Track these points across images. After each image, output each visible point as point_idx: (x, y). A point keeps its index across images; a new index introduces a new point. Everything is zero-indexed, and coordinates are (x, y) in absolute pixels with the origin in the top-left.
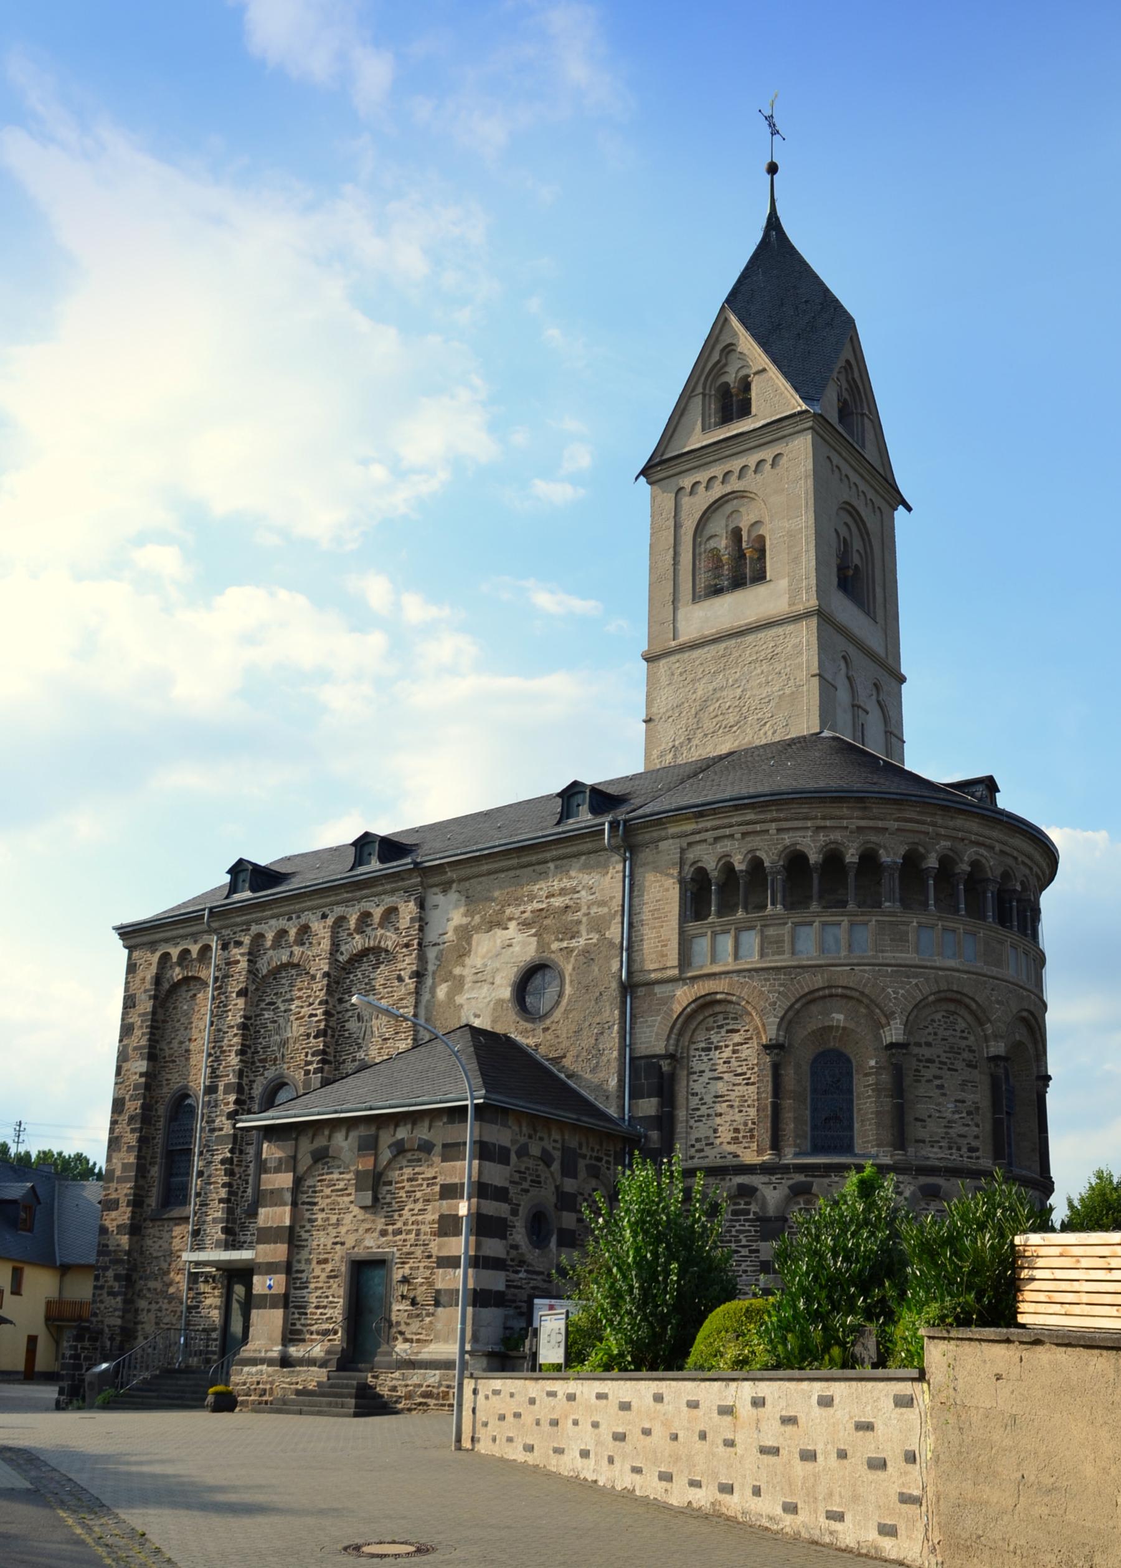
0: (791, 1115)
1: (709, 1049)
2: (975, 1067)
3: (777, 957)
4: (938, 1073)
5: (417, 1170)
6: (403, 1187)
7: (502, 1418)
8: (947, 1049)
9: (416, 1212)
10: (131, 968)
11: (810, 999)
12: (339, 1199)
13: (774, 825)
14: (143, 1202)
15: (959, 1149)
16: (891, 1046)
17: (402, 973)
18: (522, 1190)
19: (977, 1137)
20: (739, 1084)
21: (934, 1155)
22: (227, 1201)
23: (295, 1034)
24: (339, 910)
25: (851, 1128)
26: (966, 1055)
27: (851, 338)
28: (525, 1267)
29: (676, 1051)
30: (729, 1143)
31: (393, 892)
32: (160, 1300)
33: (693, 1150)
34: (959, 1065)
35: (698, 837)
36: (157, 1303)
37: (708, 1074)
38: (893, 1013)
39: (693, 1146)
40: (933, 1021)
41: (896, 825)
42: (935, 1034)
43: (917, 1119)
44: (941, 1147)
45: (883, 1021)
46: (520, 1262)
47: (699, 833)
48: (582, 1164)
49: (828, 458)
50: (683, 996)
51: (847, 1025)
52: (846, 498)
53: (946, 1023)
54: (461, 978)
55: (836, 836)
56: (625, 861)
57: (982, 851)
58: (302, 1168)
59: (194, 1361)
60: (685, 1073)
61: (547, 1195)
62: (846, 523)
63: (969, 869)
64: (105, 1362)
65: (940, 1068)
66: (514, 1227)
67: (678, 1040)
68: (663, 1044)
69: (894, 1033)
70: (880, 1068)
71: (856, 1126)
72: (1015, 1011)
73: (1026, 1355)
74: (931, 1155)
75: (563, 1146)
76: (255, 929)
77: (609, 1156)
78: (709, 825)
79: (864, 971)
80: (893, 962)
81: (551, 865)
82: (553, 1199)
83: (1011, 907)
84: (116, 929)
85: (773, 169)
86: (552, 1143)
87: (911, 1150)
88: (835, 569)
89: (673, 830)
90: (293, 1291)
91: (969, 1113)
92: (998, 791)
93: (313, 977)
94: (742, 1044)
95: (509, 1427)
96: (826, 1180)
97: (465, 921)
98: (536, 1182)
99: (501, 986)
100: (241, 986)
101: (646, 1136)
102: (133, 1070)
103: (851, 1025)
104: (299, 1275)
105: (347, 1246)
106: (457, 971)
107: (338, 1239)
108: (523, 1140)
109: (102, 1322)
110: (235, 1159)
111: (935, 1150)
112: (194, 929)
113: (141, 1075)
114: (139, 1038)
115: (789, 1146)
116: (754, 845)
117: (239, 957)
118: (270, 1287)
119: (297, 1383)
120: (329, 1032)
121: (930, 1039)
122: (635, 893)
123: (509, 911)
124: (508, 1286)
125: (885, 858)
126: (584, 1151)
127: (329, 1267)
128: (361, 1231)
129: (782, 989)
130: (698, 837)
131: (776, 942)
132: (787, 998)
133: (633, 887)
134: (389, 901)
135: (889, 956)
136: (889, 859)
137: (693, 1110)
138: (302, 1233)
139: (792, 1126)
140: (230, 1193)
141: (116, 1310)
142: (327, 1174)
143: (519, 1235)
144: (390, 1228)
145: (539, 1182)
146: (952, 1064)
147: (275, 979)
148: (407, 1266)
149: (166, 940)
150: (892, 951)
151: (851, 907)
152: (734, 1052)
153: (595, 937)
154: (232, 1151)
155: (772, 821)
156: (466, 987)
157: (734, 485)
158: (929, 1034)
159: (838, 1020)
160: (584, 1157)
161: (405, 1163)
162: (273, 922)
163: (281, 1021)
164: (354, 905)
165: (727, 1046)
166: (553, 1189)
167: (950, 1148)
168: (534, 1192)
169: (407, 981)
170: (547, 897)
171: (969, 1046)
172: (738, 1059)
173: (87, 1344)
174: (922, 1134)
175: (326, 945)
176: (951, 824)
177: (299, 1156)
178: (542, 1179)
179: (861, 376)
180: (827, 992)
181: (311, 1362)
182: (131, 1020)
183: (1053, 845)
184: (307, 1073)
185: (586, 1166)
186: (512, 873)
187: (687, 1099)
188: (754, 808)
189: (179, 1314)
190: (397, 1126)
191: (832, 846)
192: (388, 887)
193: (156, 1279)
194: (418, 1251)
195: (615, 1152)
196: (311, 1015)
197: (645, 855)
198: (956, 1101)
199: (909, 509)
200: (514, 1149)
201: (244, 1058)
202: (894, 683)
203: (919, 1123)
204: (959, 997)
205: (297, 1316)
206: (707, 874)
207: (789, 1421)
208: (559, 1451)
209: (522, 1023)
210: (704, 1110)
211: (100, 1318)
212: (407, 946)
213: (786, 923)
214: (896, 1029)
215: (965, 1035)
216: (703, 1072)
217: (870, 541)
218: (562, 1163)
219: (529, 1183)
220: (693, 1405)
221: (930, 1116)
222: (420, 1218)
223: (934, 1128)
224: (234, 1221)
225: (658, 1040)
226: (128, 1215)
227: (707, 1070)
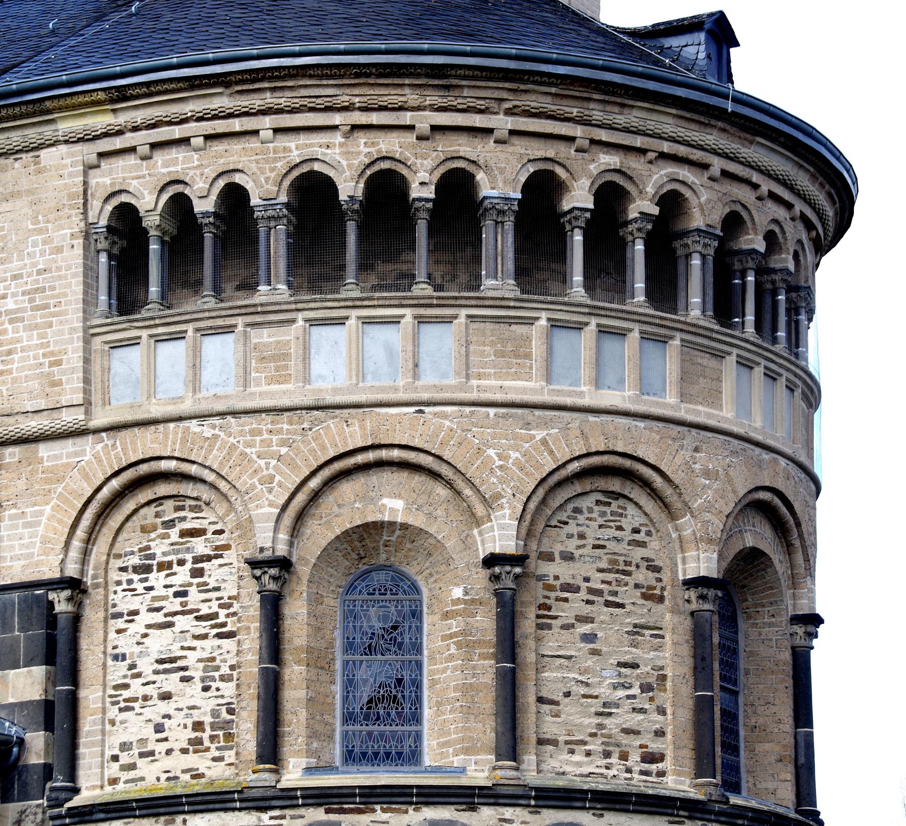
0: (301, 694)
1: (148, 569)
2: (661, 599)
3: (275, 387)
4: (587, 610)
8: (604, 565)
11: (345, 468)
13: (268, 122)
15: (624, 757)
20: (204, 637)
25: (416, 718)
26: (642, 576)
29: (82, 572)
30: (184, 751)
33: (116, 766)
34: (628, 595)
35: (118, 143)
37: (146, 618)
38: (498, 496)
39: (115, 758)
40: (577, 510)
42: (582, 536)
44: (588, 754)
45: (480, 510)
47: (120, 133)
50: (89, 464)
51: (410, 521)
55: (390, 144)
57: (685, 173)
60: (101, 615)
63: (655, 211)
65: (588, 602)
68: (55, 560)
69: (501, 535)
70: (473, 601)
71: (427, 713)
72: (741, 493)
74: (568, 769)
78: (139, 116)
79: (445, 416)
83: (744, 285)
87: (529, 759)
91: (646, 688)
92: (737, 44)
94: (209, 558)
101: (21, 742)
103: (417, 520)
111: (577, 758)
115: (297, 754)
116: (231, 161)
121: (571, 545)
125: (488, 188)
129: (283, 450)
130: (118, 143)
131: (274, 358)
135: (492, 386)
136: (494, 193)
137: (116, 687)
139: (303, 714)
146: (615, 594)
150: (498, 376)
151: (421, 289)
152: (197, 573)
159: (392, 510)
165: (181, 563)
167: (607, 755)
171: (647, 560)
172: (204, 588)
174: (551, 727)
176: (621, 119)
183: (839, 156)
187: (105, 665)
188: (227, 85)
198: (620, 664)
203: (546, 708)
204: (627, 463)
206: (140, 219)
210: (137, 688)
213: (293, 321)
214: (502, 527)
216: (135, 613)
221: (567, 694)
223: (576, 718)
227: (143, 609)
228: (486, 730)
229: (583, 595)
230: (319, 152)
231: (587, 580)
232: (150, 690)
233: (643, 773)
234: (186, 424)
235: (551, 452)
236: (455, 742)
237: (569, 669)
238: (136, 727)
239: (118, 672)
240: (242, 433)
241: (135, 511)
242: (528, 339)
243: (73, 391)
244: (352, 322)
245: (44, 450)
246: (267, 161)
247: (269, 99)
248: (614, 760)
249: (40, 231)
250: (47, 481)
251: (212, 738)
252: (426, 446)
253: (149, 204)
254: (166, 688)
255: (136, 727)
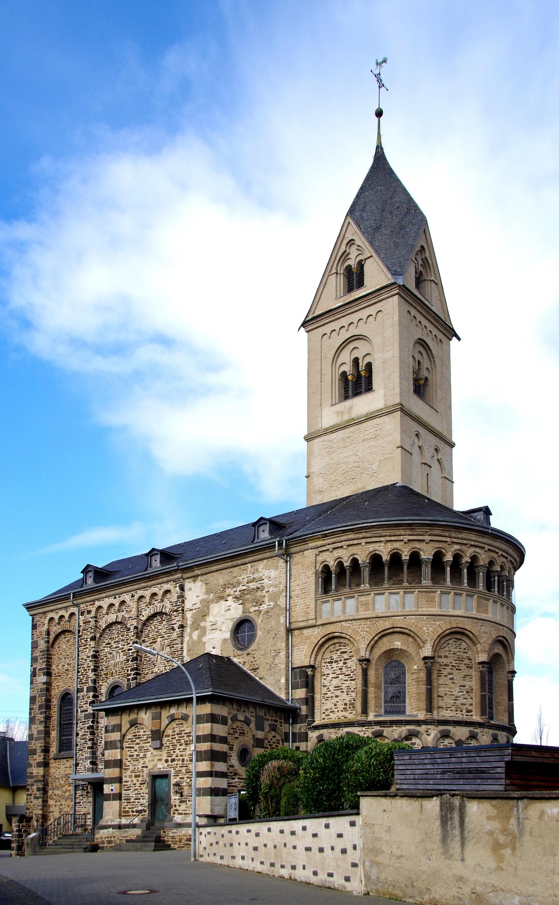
0: (373, 695)
1: (332, 662)
2: (472, 668)
5: (181, 729)
6: (175, 738)
7: (211, 844)
8: (456, 659)
9: (181, 750)
10: (34, 627)
11: (384, 634)
12: (144, 745)
13: (364, 540)
14: (49, 750)
15: (461, 711)
16: (425, 658)
17: (174, 626)
18: (235, 738)
19: (471, 705)
20: (347, 680)
21: (447, 714)
22: (92, 748)
23: (121, 660)
24: (140, 593)
25: (404, 702)
26: (467, 661)
27: (424, 231)
28: (238, 776)
29: (315, 664)
30: (342, 711)
31: (167, 582)
32: (61, 800)
33: (324, 715)
34: (463, 667)
35: (324, 548)
36: (60, 801)
37: (331, 676)
38: (427, 640)
39: (324, 713)
40: (448, 644)
41: (429, 538)
42: (450, 651)
43: (438, 696)
44: (451, 710)
45: (421, 644)
46: (235, 773)
47: (325, 546)
48: (267, 724)
49: (409, 312)
50: (317, 634)
51: (402, 648)
52: (420, 337)
53: (456, 645)
54: (205, 627)
55: (397, 545)
56: (287, 562)
57: (478, 550)
58: (124, 730)
59: (79, 830)
60: (320, 675)
61: (248, 740)
62: (420, 352)
63: (470, 560)
64: (34, 832)
66: (231, 756)
67: (316, 658)
68: (308, 660)
69: (427, 651)
70: (420, 670)
71: (407, 700)
72: (494, 637)
73: (393, 801)
74: (446, 715)
75: (256, 715)
76: (97, 604)
77: (281, 719)
78: (330, 541)
79: (412, 619)
80: (427, 613)
81: (249, 565)
82: (252, 742)
83: (494, 580)
84: (24, 605)
85: (379, 114)
86: (250, 714)
87: (435, 712)
88: (412, 381)
89: (311, 545)
90: (123, 792)
91: (467, 692)
93: (129, 629)
94: (348, 659)
95: (214, 849)
96: (391, 729)
97: (205, 597)
98: (242, 733)
99: (225, 631)
100: (92, 635)
101: (300, 709)
102: (39, 681)
103: (404, 648)
104: (126, 784)
105: (149, 768)
106: (202, 624)
107: (144, 765)
108: (234, 712)
109: (32, 812)
110: (95, 726)
111: (448, 712)
112: (65, 605)
113: (44, 683)
114: (41, 665)
117: (90, 619)
118: (112, 790)
119: (127, 837)
120: (139, 658)
121: (447, 654)
122: (292, 580)
123: (228, 591)
124: (228, 786)
125: (423, 556)
126: (268, 717)
127: (140, 779)
128: (155, 761)
129: (368, 629)
130: (324, 548)
131: (365, 604)
132: (370, 633)
133: (289, 575)
134: (166, 587)
135: (425, 610)
136: (425, 557)
137: (324, 694)
138: (127, 762)
139: (374, 701)
140: (93, 744)
141: (38, 806)
142: (138, 732)
143: (234, 760)
144: (170, 759)
145: (244, 734)
146: (459, 667)
147: (110, 630)
148: (178, 777)
149: (51, 611)
150: (426, 607)
151: (406, 584)
152: (345, 663)
153: (272, 604)
154: (93, 722)
155: (362, 538)
156: (207, 633)
157: (353, 331)
158: (446, 651)
160: (268, 720)
161: (175, 726)
162: (106, 600)
163: (114, 653)
164: (148, 590)
165: (341, 660)
166: (251, 737)
167: (457, 711)
168: (241, 738)
169: (177, 630)
170: (247, 583)
173: (24, 824)
174: (441, 704)
175: (134, 613)
177: (123, 724)
178: (245, 732)
179: (430, 255)
180: (391, 630)
181: (134, 826)
182: (36, 655)
184: (128, 680)
185: (269, 725)
186: (229, 570)
188: (353, 531)
189: (71, 806)
190: (170, 707)
191: (395, 551)
192: (165, 579)
193: (58, 789)
194: (184, 770)
195: (285, 717)
196: (129, 650)
197: (297, 558)
198: (460, 686)
199: (459, 339)
200: (229, 717)
201: (96, 673)
202: (447, 448)
203: (440, 698)
205: (126, 804)
206: (330, 568)
207: (315, 835)
208: (233, 857)
209: (236, 651)
210: (329, 694)
211: (30, 811)
212: (176, 611)
213: (370, 594)
214: (428, 649)
215: (466, 651)
216: (329, 674)
217: (434, 361)
218: (256, 723)
219: (238, 734)
220: (282, 832)
221: (446, 694)
222: (184, 753)
223: (448, 701)
224: (96, 758)
225: (305, 658)
226: (42, 757)
228: (423, 705)
229: (450, 667)
230: (377, 548)
231: (451, 663)
232: (333, 695)
233: (466, 715)
234: (342, 623)
235: (441, 628)
236: (415, 708)
237: (446, 688)
238: (329, 705)
239: (324, 690)
240: (357, 625)
241: (328, 647)
242: (435, 597)
243: (312, 615)
244: (386, 594)
245: (305, 631)
246: (364, 551)
247: (364, 535)
248: (459, 712)
249: (304, 573)
250: (305, 639)
251: (349, 708)
252: (407, 627)
253: (332, 564)
254: (337, 694)
255: (329, 705)
